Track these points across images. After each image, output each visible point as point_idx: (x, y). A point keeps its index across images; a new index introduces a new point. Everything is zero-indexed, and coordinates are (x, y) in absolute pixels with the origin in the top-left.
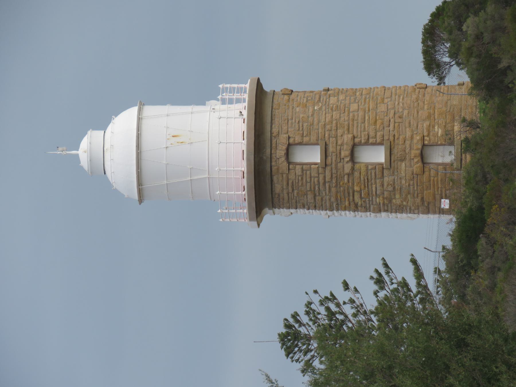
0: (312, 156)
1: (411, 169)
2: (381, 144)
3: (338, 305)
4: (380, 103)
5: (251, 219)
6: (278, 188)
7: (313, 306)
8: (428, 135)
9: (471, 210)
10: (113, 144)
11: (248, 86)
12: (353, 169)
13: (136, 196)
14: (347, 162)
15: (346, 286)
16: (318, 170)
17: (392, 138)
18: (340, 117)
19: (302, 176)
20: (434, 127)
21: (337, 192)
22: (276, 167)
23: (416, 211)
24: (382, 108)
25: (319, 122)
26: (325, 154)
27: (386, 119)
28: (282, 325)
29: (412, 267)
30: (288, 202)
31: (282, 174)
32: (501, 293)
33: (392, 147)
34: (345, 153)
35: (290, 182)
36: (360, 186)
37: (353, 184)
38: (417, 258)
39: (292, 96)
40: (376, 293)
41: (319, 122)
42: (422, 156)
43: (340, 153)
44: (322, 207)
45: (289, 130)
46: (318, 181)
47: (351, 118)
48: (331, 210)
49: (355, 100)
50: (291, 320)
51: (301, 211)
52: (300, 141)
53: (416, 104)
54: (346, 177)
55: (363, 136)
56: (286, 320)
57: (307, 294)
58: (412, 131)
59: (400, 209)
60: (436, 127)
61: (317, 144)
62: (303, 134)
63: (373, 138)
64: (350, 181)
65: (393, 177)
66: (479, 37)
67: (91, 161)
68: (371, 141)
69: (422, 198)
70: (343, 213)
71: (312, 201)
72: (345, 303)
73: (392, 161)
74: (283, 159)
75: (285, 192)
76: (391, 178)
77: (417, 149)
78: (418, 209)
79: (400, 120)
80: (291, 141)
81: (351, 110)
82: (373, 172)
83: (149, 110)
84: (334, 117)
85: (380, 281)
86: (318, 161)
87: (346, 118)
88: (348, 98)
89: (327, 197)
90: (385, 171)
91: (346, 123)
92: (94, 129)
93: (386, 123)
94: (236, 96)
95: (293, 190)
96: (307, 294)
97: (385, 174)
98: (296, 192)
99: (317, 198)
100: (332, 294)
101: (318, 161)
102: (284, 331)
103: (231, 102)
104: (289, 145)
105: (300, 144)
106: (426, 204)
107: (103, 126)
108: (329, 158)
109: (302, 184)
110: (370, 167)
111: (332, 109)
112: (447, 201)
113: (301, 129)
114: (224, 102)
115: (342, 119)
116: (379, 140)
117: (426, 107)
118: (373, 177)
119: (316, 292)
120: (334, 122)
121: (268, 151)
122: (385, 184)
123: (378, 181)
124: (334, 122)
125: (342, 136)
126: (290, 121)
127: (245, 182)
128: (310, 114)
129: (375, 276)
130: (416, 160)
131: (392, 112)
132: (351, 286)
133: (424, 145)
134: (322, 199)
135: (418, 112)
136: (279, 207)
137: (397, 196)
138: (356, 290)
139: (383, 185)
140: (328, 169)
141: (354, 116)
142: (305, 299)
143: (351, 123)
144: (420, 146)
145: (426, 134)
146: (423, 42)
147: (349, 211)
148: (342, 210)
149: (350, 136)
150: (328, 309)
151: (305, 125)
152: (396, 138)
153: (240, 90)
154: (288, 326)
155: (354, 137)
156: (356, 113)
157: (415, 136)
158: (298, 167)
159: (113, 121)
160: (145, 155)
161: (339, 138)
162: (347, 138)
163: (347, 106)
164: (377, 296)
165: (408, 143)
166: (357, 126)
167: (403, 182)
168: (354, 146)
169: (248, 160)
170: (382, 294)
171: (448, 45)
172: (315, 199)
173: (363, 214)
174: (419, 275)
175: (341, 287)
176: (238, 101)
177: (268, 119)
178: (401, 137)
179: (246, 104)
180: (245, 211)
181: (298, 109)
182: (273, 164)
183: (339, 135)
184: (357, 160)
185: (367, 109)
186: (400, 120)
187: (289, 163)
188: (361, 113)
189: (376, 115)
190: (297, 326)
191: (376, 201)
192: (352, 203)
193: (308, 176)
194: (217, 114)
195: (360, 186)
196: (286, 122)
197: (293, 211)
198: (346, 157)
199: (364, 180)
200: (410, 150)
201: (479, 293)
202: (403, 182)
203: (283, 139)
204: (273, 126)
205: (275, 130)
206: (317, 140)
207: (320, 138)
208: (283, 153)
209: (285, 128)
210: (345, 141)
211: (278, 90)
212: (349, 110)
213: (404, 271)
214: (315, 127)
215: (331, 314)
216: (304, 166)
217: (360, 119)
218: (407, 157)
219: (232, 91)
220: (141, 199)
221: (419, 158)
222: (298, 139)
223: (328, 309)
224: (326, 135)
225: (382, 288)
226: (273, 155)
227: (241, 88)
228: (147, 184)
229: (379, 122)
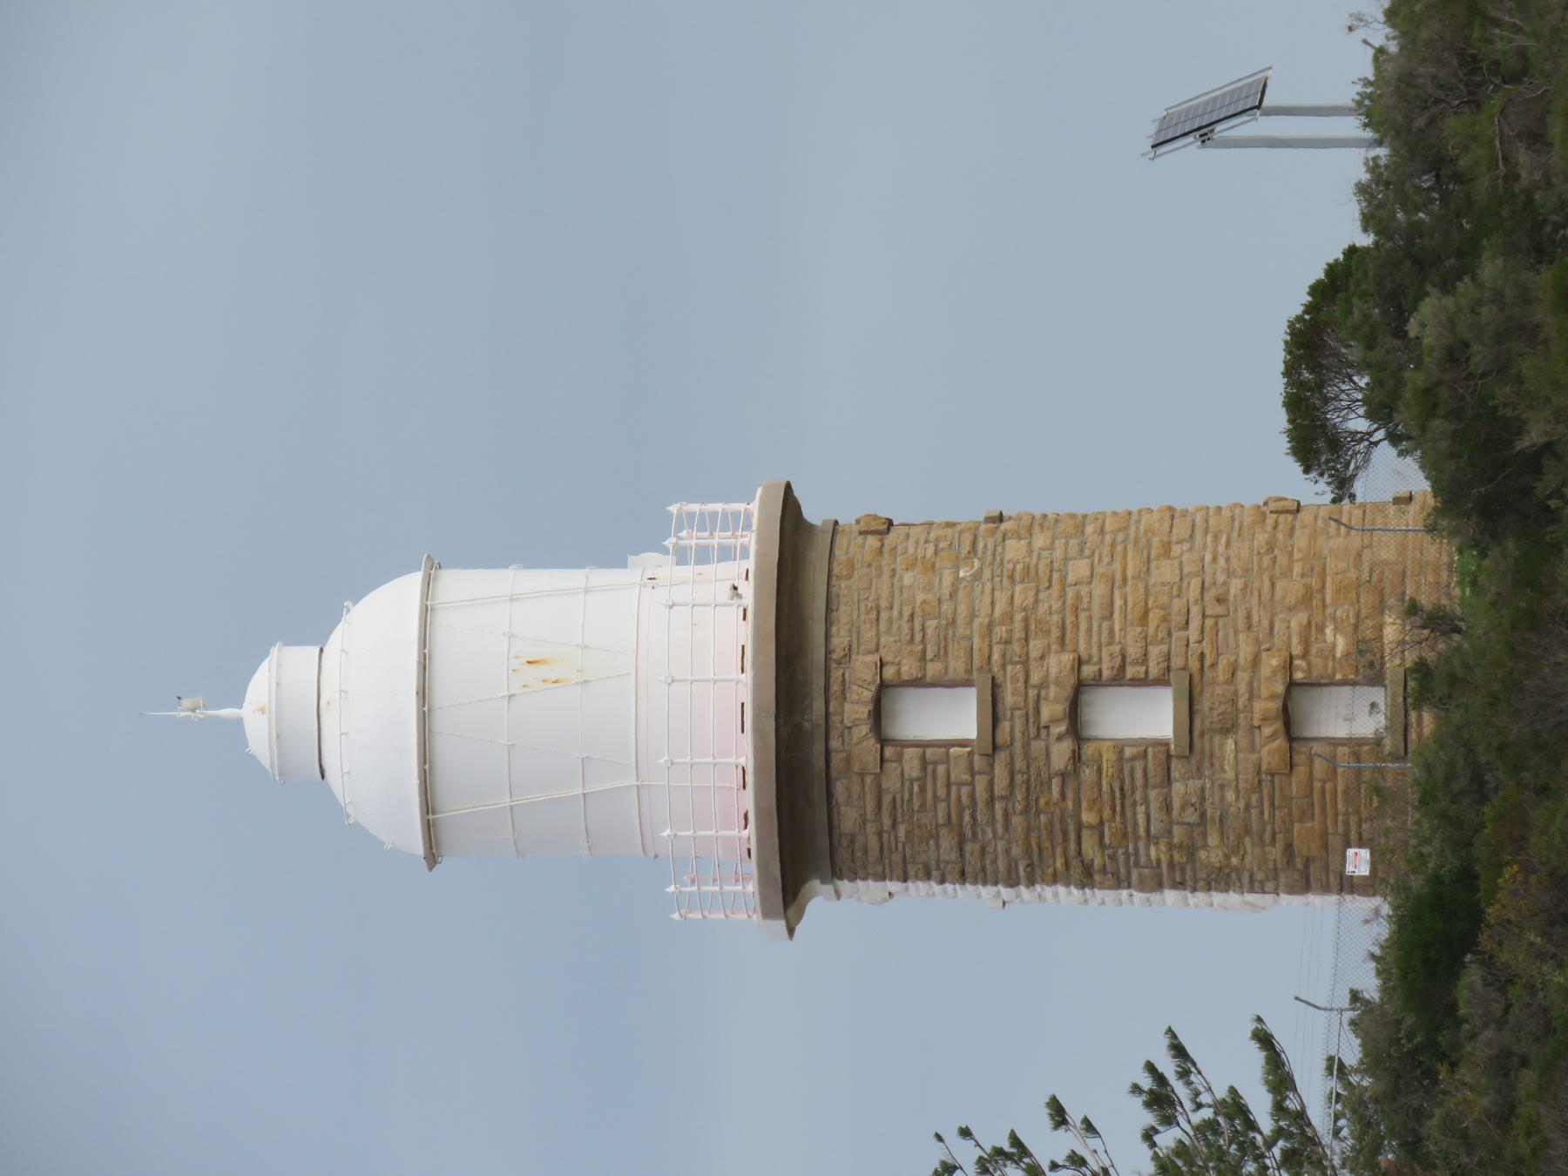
0: (950, 718)
1: (1255, 756)
2: (1162, 681)
4: (1158, 558)
5: (767, 913)
6: (848, 818)
8: (1305, 655)
9: (1436, 880)
10: (347, 690)
11: (754, 507)
12: (1076, 757)
14: (1060, 738)
15: (1059, 1115)
17: (1194, 665)
18: (1037, 601)
19: (922, 780)
20: (1321, 629)
21: (1029, 829)
22: (843, 755)
23: (1269, 886)
24: (1165, 572)
25: (973, 615)
26: (993, 713)
27: (1178, 604)
29: (1258, 1057)
30: (881, 860)
31: (862, 775)
32: (1529, 1134)
33: (1196, 691)
34: (1052, 709)
35: (887, 800)
36: (1100, 811)
37: (1078, 804)
38: (1272, 1027)
39: (891, 539)
40: (1149, 1136)
41: (973, 615)
42: (1288, 718)
43: (1037, 710)
45: (883, 640)
46: (972, 796)
47: (1069, 602)
48: (1012, 882)
51: (919, 889)
52: (916, 673)
53: (1266, 561)
54: (1056, 782)
55: (1105, 658)
57: (939, 1138)
58: (1258, 642)
59: (1221, 879)
60: (1329, 631)
61: (968, 683)
62: (924, 652)
64: (1070, 794)
65: (1198, 783)
66: (1455, 355)
68: (1131, 671)
69: (1289, 847)
70: (1048, 891)
71: (953, 856)
73: (1196, 733)
74: (864, 729)
76: (1195, 784)
77: (1272, 697)
78: (1276, 878)
79: (1219, 609)
80: (889, 673)
81: (1070, 579)
82: (1139, 766)
83: (456, 584)
84: (1017, 601)
85: (1160, 1100)
86: (972, 734)
87: (1056, 605)
88: (1059, 543)
89: (1001, 845)
90: (1174, 763)
91: (1055, 618)
92: (288, 643)
93: (1177, 620)
94: (718, 539)
95: (894, 825)
96: (939, 1138)
97: (1175, 774)
98: (902, 829)
99: (968, 847)
100: (1015, 1141)
101: (972, 734)
103: (703, 556)
105: (918, 683)
106: (1299, 863)
107: (315, 627)
108: (1005, 725)
109: (923, 805)
110: (1128, 752)
111: (1012, 577)
112: (1365, 854)
113: (918, 637)
114: (681, 557)
115: (1043, 608)
116: (1154, 672)
117: (1297, 570)
119: (965, 1133)
120: (1019, 617)
121: (818, 705)
122: (1176, 804)
123: (1153, 794)
124: (1019, 617)
125: (1042, 657)
126: (884, 615)
127: (748, 800)
128: (946, 592)
129: (1147, 1083)
130: (1267, 731)
131: (1195, 583)
132: (1074, 1115)
133: (1292, 685)
134: (983, 851)
137: (1213, 840)
138: (1089, 1127)
139: (1168, 807)
140: (1002, 757)
141: (1078, 597)
143: (1069, 619)
144: (1280, 688)
145: (1297, 650)
146: (1290, 371)
147: (1067, 884)
149: (1067, 658)
152: (1208, 662)
153: (731, 522)
155: (1080, 662)
156: (1084, 590)
157: (1264, 655)
159: (346, 617)
161: (1033, 664)
162: (1059, 663)
163: (1056, 566)
164: (1153, 1145)
165: (1243, 677)
166: (1089, 630)
167: (1230, 796)
168: (1080, 687)
170: (1167, 1139)
171: (1363, 382)
172: (961, 850)
173: (1109, 895)
174: (1280, 1079)
175: (1044, 1114)
176: (726, 554)
177: (818, 631)
178: (1223, 661)
179: (750, 564)
180: (751, 887)
181: (908, 578)
182: (835, 744)
183: (1034, 654)
185: (1118, 577)
186: (1219, 609)
187: (883, 741)
188: (1099, 589)
189: (1147, 594)
191: (1148, 855)
192: (1075, 863)
193: (941, 782)
196: (873, 615)
197: (893, 886)
198: (1057, 721)
199: (1112, 791)
200: (1251, 698)
201: (1464, 1135)
202: (1230, 796)
203: (863, 668)
204: (834, 629)
205: (840, 641)
206: (969, 671)
207: (976, 664)
208: (864, 711)
209: (869, 634)
211: (847, 519)
212: (1063, 579)
213: (1232, 1069)
216: (929, 752)
217: (1096, 604)
218: (1242, 720)
219: (707, 523)
220: (432, 856)
221: (1279, 725)
222: (909, 669)
224: (996, 656)
225: (1169, 1121)
226: (835, 719)
227: (736, 515)
228: (451, 808)
229: (1154, 617)
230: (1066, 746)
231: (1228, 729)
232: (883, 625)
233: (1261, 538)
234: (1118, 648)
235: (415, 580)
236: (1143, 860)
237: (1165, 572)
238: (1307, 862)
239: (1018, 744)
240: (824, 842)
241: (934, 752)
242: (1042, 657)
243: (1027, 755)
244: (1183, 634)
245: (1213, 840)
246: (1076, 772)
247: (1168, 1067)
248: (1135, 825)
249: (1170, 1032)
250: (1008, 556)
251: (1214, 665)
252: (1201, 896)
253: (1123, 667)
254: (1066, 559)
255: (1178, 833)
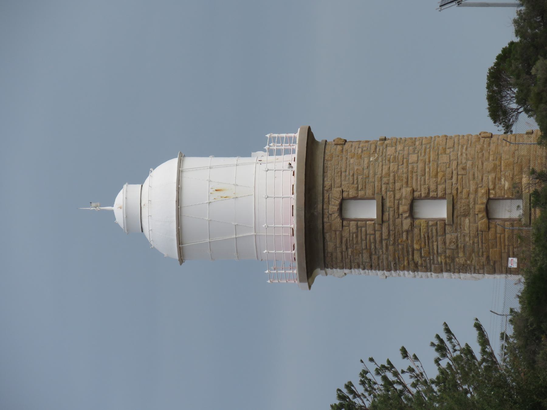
0: (368, 211)
1: (476, 225)
2: (443, 198)
3: (396, 374)
5: (301, 281)
6: (330, 246)
7: (368, 376)
8: (494, 189)
10: (151, 199)
11: (297, 135)
12: (412, 225)
13: (176, 255)
14: (406, 218)
15: (404, 353)
16: (374, 227)
17: (454, 192)
18: (398, 169)
19: (357, 233)
20: (500, 179)
23: (481, 271)
24: (444, 159)
25: (375, 174)
27: (449, 170)
28: (335, 395)
29: (475, 333)
30: (342, 261)
31: (335, 231)
33: (455, 201)
34: (404, 208)
36: (420, 244)
37: (412, 241)
38: (482, 322)
39: (346, 146)
40: (437, 361)
41: (375, 174)
42: (488, 211)
43: (398, 208)
44: (379, 267)
45: (343, 183)
47: (410, 169)
48: (389, 270)
49: (414, 151)
50: (345, 391)
51: (355, 271)
53: (480, 155)
54: (404, 235)
55: (423, 189)
56: (339, 390)
57: (362, 361)
58: (477, 184)
59: (464, 269)
60: (503, 180)
62: (358, 187)
63: (433, 191)
64: (409, 238)
67: (127, 217)
68: (432, 194)
69: (488, 257)
70: (401, 273)
71: (368, 260)
72: (403, 372)
73: (455, 216)
74: (336, 215)
75: (338, 250)
77: (482, 204)
78: (483, 269)
79: (463, 172)
80: (345, 194)
81: (410, 161)
83: (190, 162)
84: (391, 169)
85: (441, 348)
86: (375, 217)
87: (405, 170)
88: (406, 148)
89: (385, 256)
90: (447, 227)
91: (405, 175)
93: (448, 176)
94: (284, 146)
95: (347, 248)
96: (362, 361)
97: (447, 231)
98: (350, 251)
99: (373, 257)
100: (389, 362)
102: (338, 402)
103: (279, 153)
104: (343, 199)
105: (355, 198)
106: (492, 264)
107: (140, 179)
110: (431, 223)
111: (389, 161)
112: (515, 260)
113: (355, 182)
114: (271, 153)
116: (440, 194)
118: (434, 234)
119: (371, 360)
120: (392, 175)
121: (320, 206)
122: (448, 242)
123: (439, 238)
124: (392, 175)
125: (400, 189)
126: (343, 174)
127: (294, 240)
129: (436, 342)
131: (455, 163)
132: (410, 353)
133: (489, 199)
134: (378, 258)
135: (482, 164)
136: (332, 267)
137: (461, 255)
138: (416, 358)
139: (444, 243)
140: (385, 225)
141: (413, 168)
142: (360, 368)
143: (410, 175)
144: (485, 201)
145: (491, 187)
146: (489, 87)
147: (408, 271)
148: (400, 269)
149: (409, 189)
150: (385, 378)
151: (360, 177)
152: (459, 191)
153: (289, 140)
154: (342, 397)
155: (413, 191)
156: (415, 165)
157: (479, 189)
158: (352, 223)
160: (186, 211)
161: (397, 192)
162: (406, 191)
163: (405, 156)
165: (472, 196)
167: (467, 239)
169: (298, 216)
170: (444, 363)
172: (371, 258)
173: (424, 274)
174: (484, 341)
175: (399, 355)
176: (287, 152)
178: (465, 191)
179: (295, 155)
180: (295, 271)
184: (417, 216)
185: (427, 160)
186: (463, 172)
187: (343, 219)
188: (420, 165)
189: (437, 167)
190: (351, 397)
193: (364, 234)
194: (264, 167)
195: (420, 244)
196: (339, 174)
197: (346, 271)
198: (405, 212)
199: (425, 237)
200: (474, 204)
202: (467, 239)
203: (336, 193)
205: (327, 183)
206: (373, 194)
207: (376, 192)
208: (336, 208)
209: (338, 181)
210: (404, 195)
212: (408, 161)
213: (467, 337)
214: (371, 180)
215: (388, 383)
216: (359, 223)
217: (419, 170)
218: (471, 212)
219: (280, 141)
220: (181, 260)
222: (352, 193)
223: (385, 378)
224: (383, 189)
225: (444, 356)
226: (326, 211)
228: (188, 243)
229: (440, 175)
230: (409, 221)
231: (466, 215)
232: (343, 179)
233: (479, 147)
234: (427, 186)
235: (175, 161)
236: (436, 262)
237: (444, 159)
238: (495, 263)
239: (391, 220)
240: (321, 255)
241: (361, 223)
242: (400, 189)
243: (394, 224)
244: (450, 181)
245: (461, 255)
246: (412, 230)
247: (444, 336)
248: (433, 249)
249: (445, 324)
250: (388, 153)
251: (461, 192)
252: (457, 275)
253: (429, 193)
254: (408, 154)
255: (448, 252)
